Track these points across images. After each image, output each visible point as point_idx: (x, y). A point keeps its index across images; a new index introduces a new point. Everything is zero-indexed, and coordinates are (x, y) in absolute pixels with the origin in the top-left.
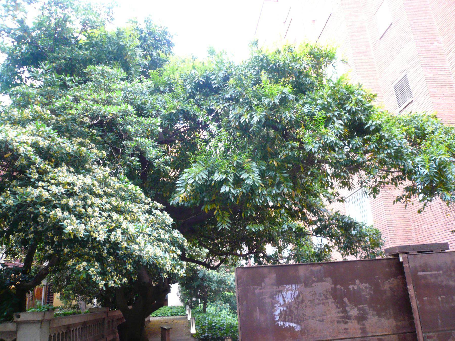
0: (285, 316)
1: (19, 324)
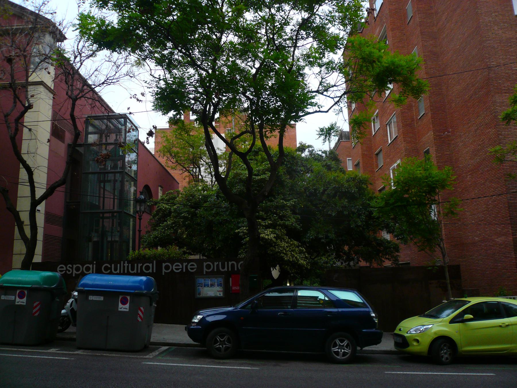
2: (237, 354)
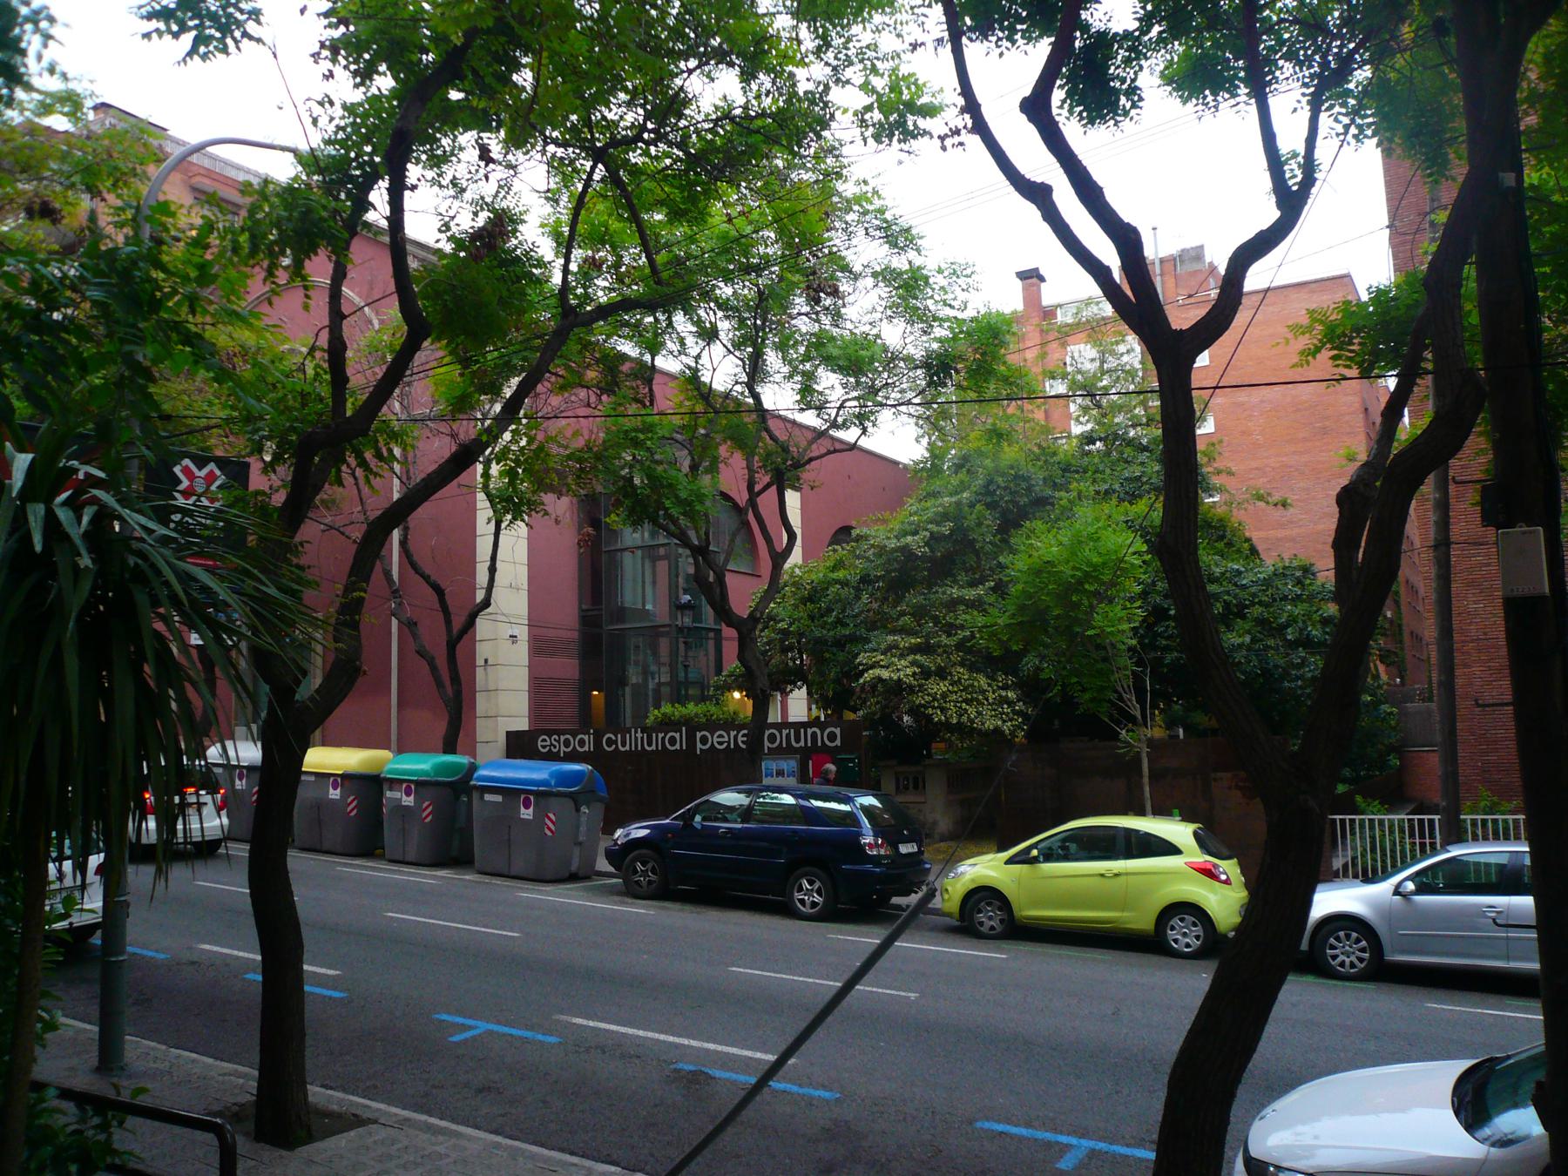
2: (663, 893)
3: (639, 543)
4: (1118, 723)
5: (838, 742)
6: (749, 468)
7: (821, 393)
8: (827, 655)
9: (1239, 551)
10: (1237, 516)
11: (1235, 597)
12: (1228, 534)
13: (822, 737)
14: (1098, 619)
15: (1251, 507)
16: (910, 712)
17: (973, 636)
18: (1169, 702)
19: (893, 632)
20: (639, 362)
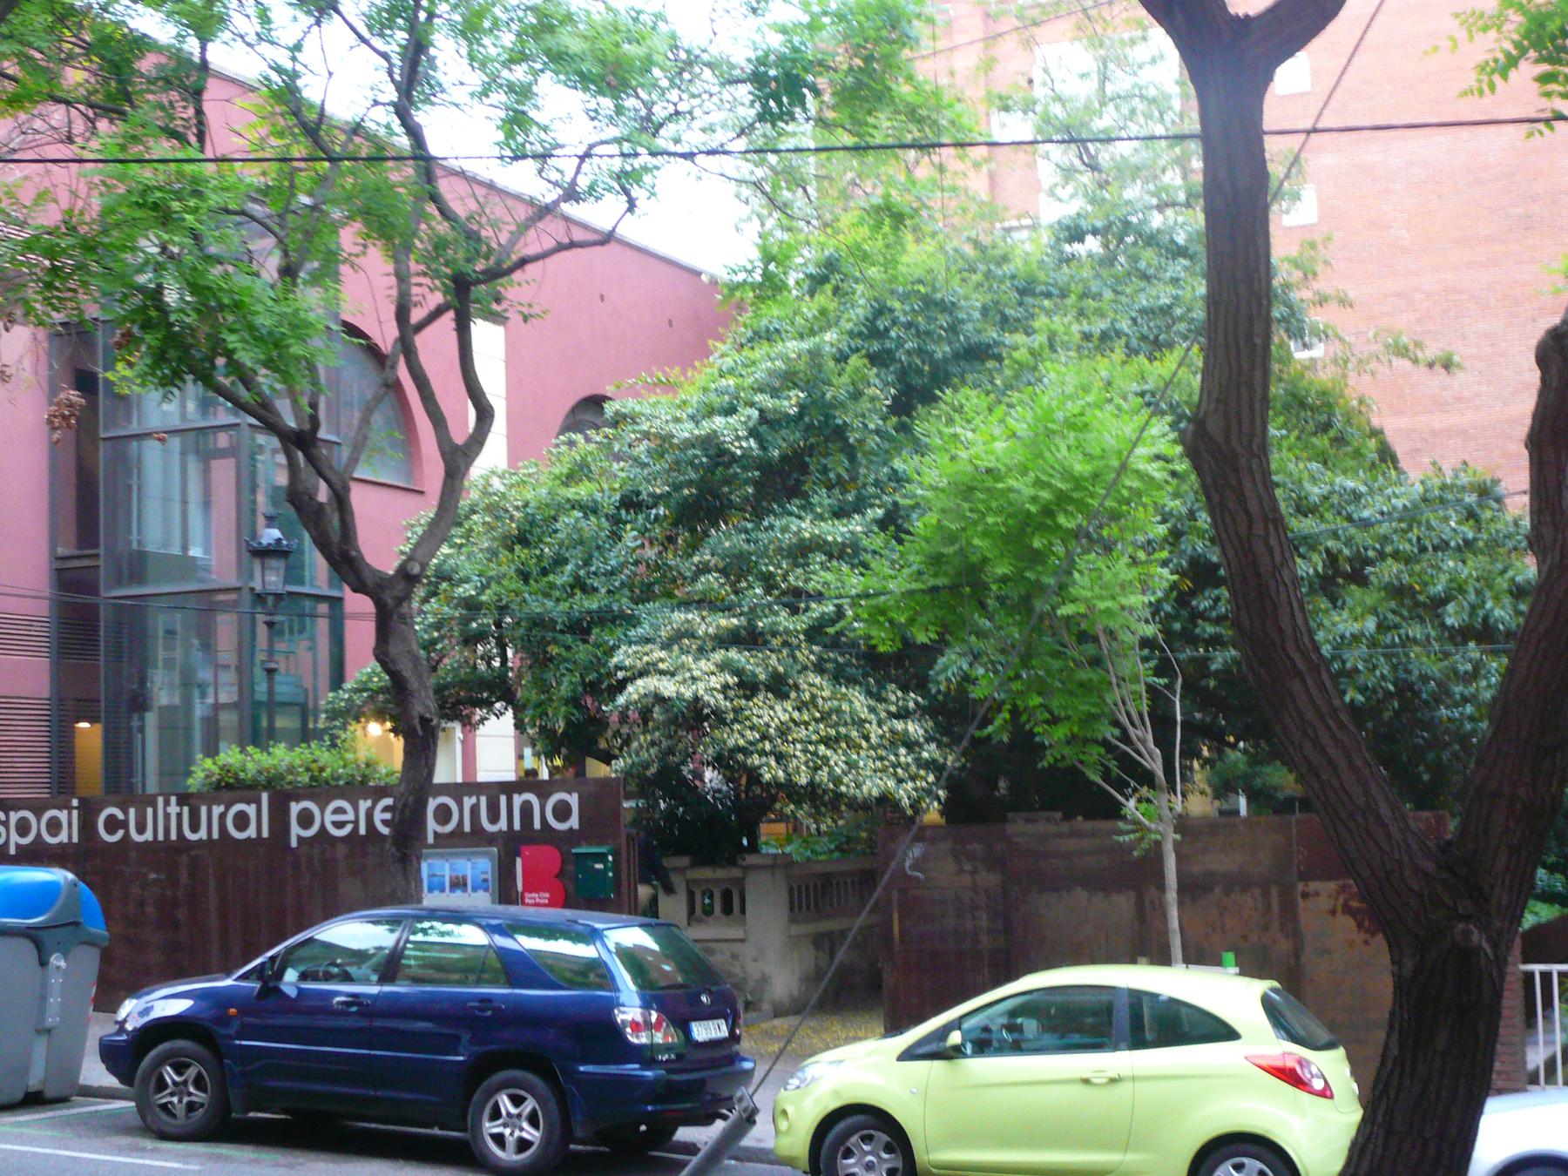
0: (913, 868)
1: (746, 869)
3: (176, 423)
4: (1121, 786)
5: (574, 822)
6: (402, 278)
7: (545, 129)
8: (554, 650)
9: (1357, 454)
10: (1357, 386)
11: (1349, 542)
12: (1338, 421)
13: (543, 812)
14: (1081, 583)
15: (1383, 370)
16: (720, 762)
17: (840, 613)
18: (1219, 744)
19: (685, 604)
20: (179, 58)
